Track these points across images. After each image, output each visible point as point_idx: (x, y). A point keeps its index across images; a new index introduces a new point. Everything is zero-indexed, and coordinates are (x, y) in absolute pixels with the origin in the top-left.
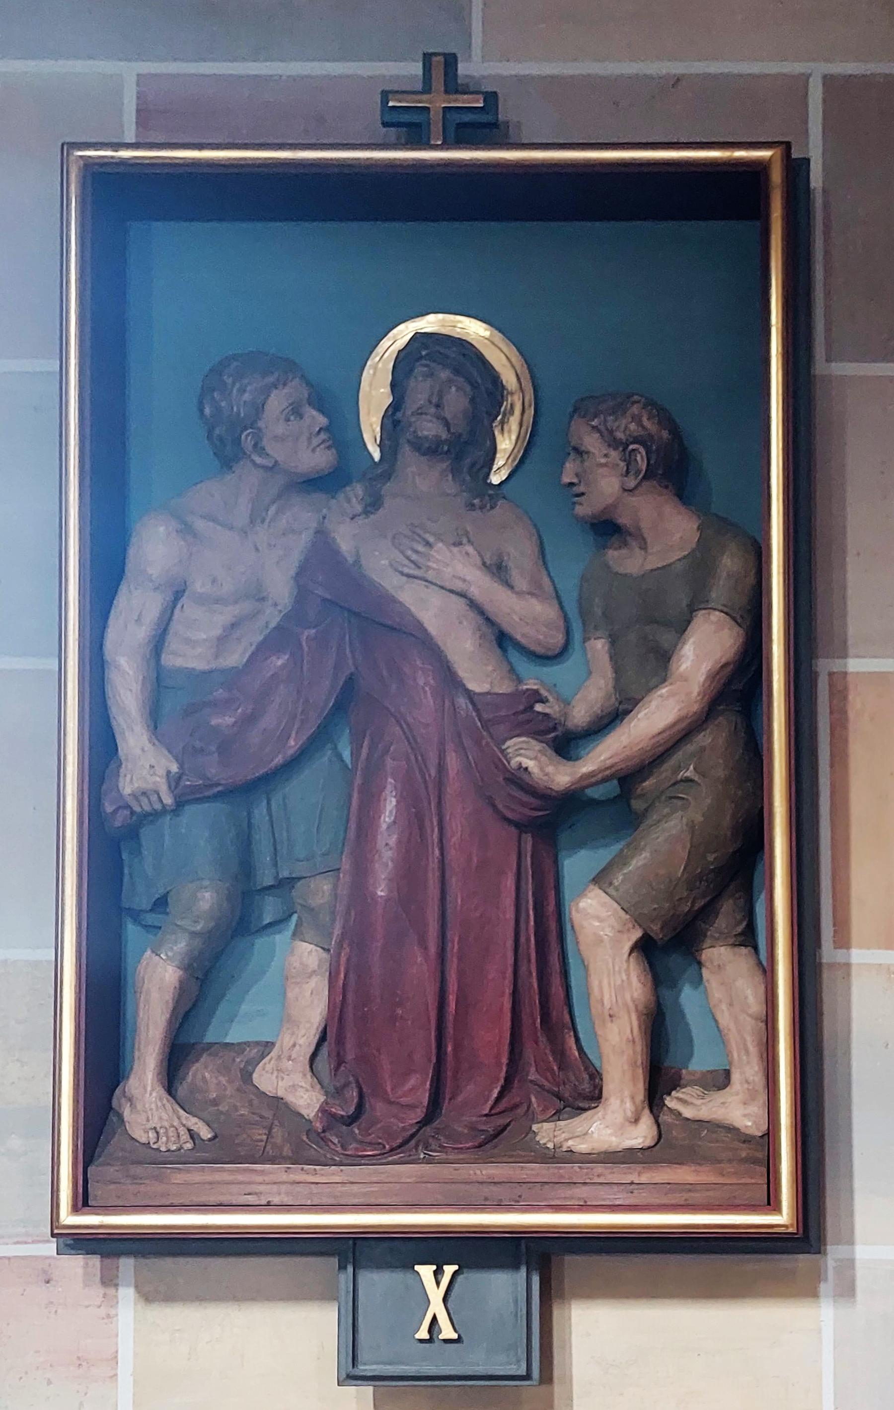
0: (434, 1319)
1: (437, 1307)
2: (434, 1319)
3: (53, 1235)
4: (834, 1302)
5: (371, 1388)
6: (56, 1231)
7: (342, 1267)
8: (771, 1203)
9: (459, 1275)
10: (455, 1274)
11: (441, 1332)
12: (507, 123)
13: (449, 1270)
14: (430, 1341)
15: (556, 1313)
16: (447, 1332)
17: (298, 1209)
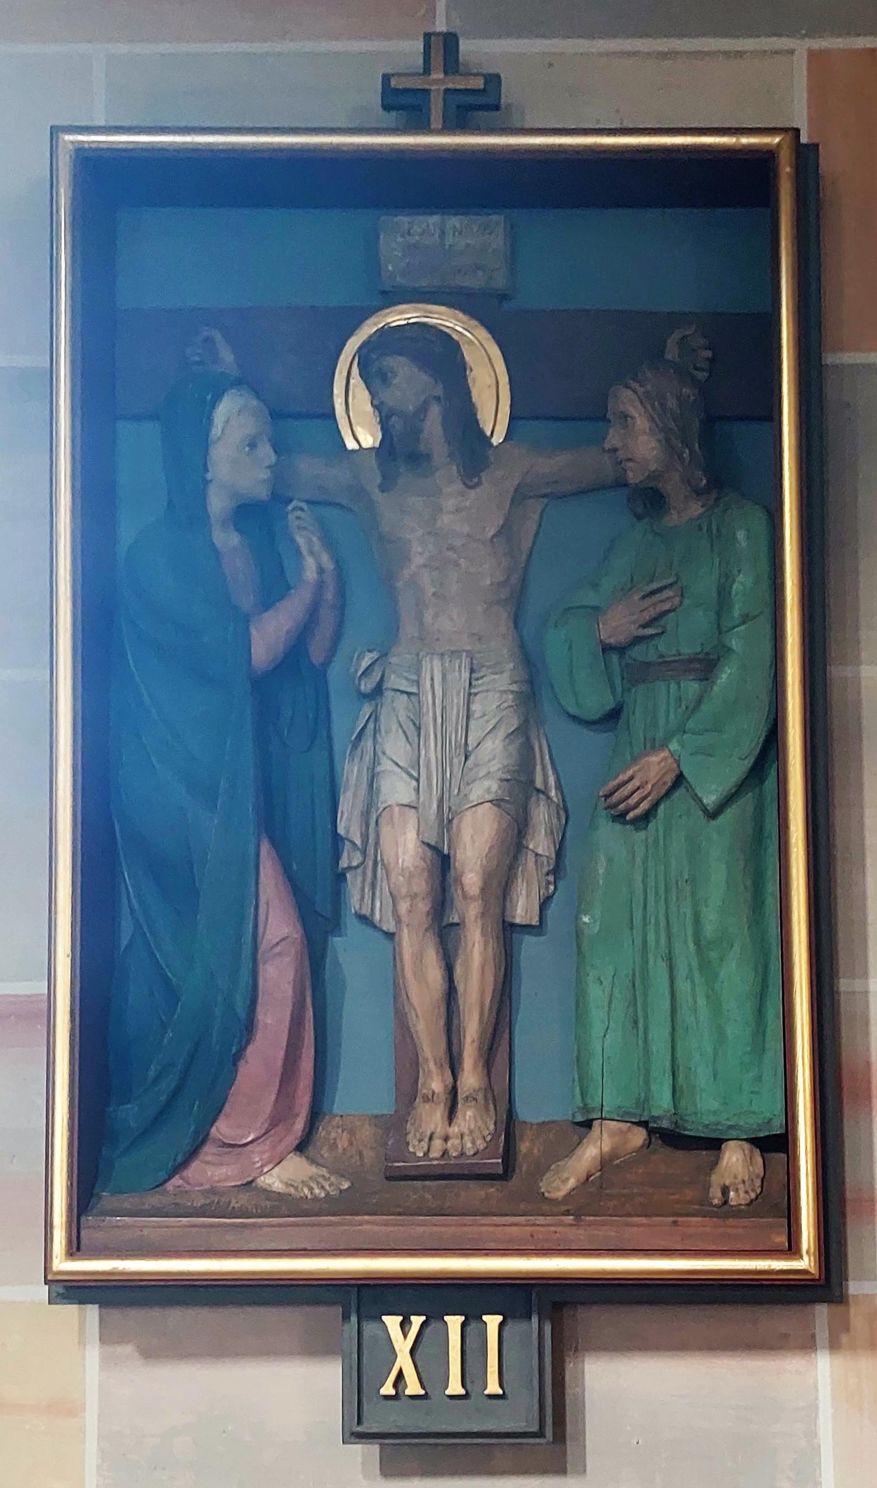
0: (400, 1374)
1: (404, 1362)
3: (46, 1283)
6: (49, 1277)
7: (346, 1317)
8: (792, 1249)
9: (427, 1326)
10: (423, 1325)
12: (509, 106)
13: (417, 1321)
15: (570, 1366)
16: (413, 1387)
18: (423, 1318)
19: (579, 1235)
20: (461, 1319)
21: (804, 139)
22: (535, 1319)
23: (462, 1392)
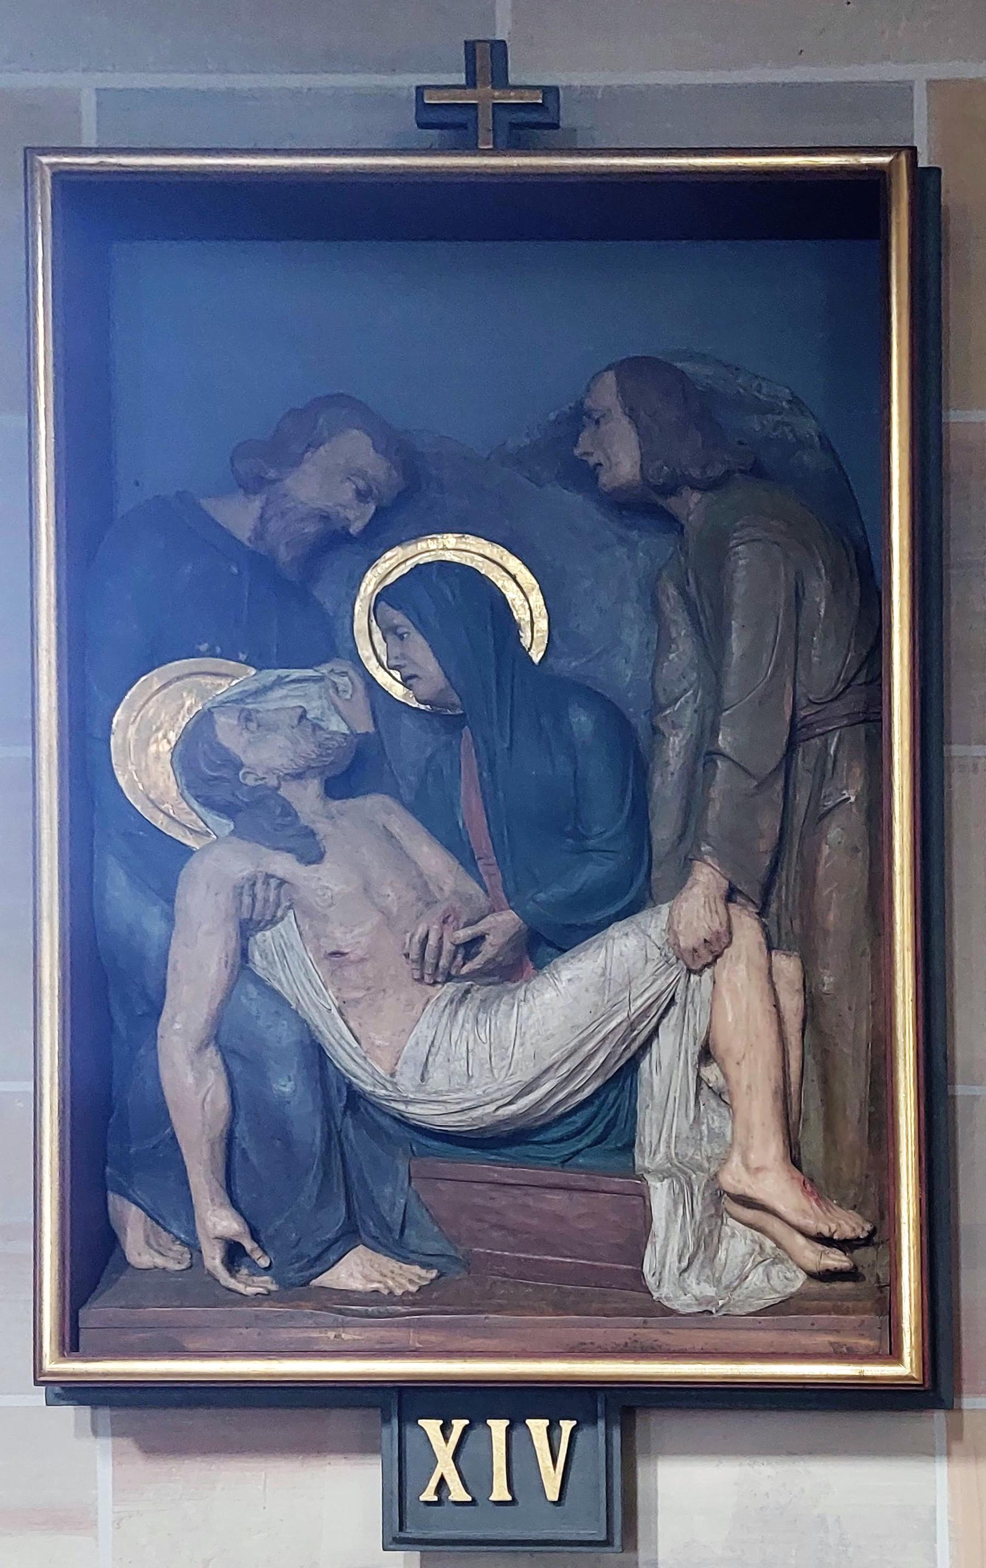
0: (442, 1480)
1: (446, 1467)
2: (442, 1480)
3: (37, 1383)
4: (949, 1461)
5: (418, 1553)
8: (894, 1355)
10: (466, 1430)
11: (450, 1494)
13: (459, 1425)
14: (438, 1503)
16: (458, 1493)
17: (237, 1355)
18: (574, 1423)
19: (413, 1339)
20: (506, 1423)
21: (923, 163)
22: (601, 1424)
23: (508, 1498)
